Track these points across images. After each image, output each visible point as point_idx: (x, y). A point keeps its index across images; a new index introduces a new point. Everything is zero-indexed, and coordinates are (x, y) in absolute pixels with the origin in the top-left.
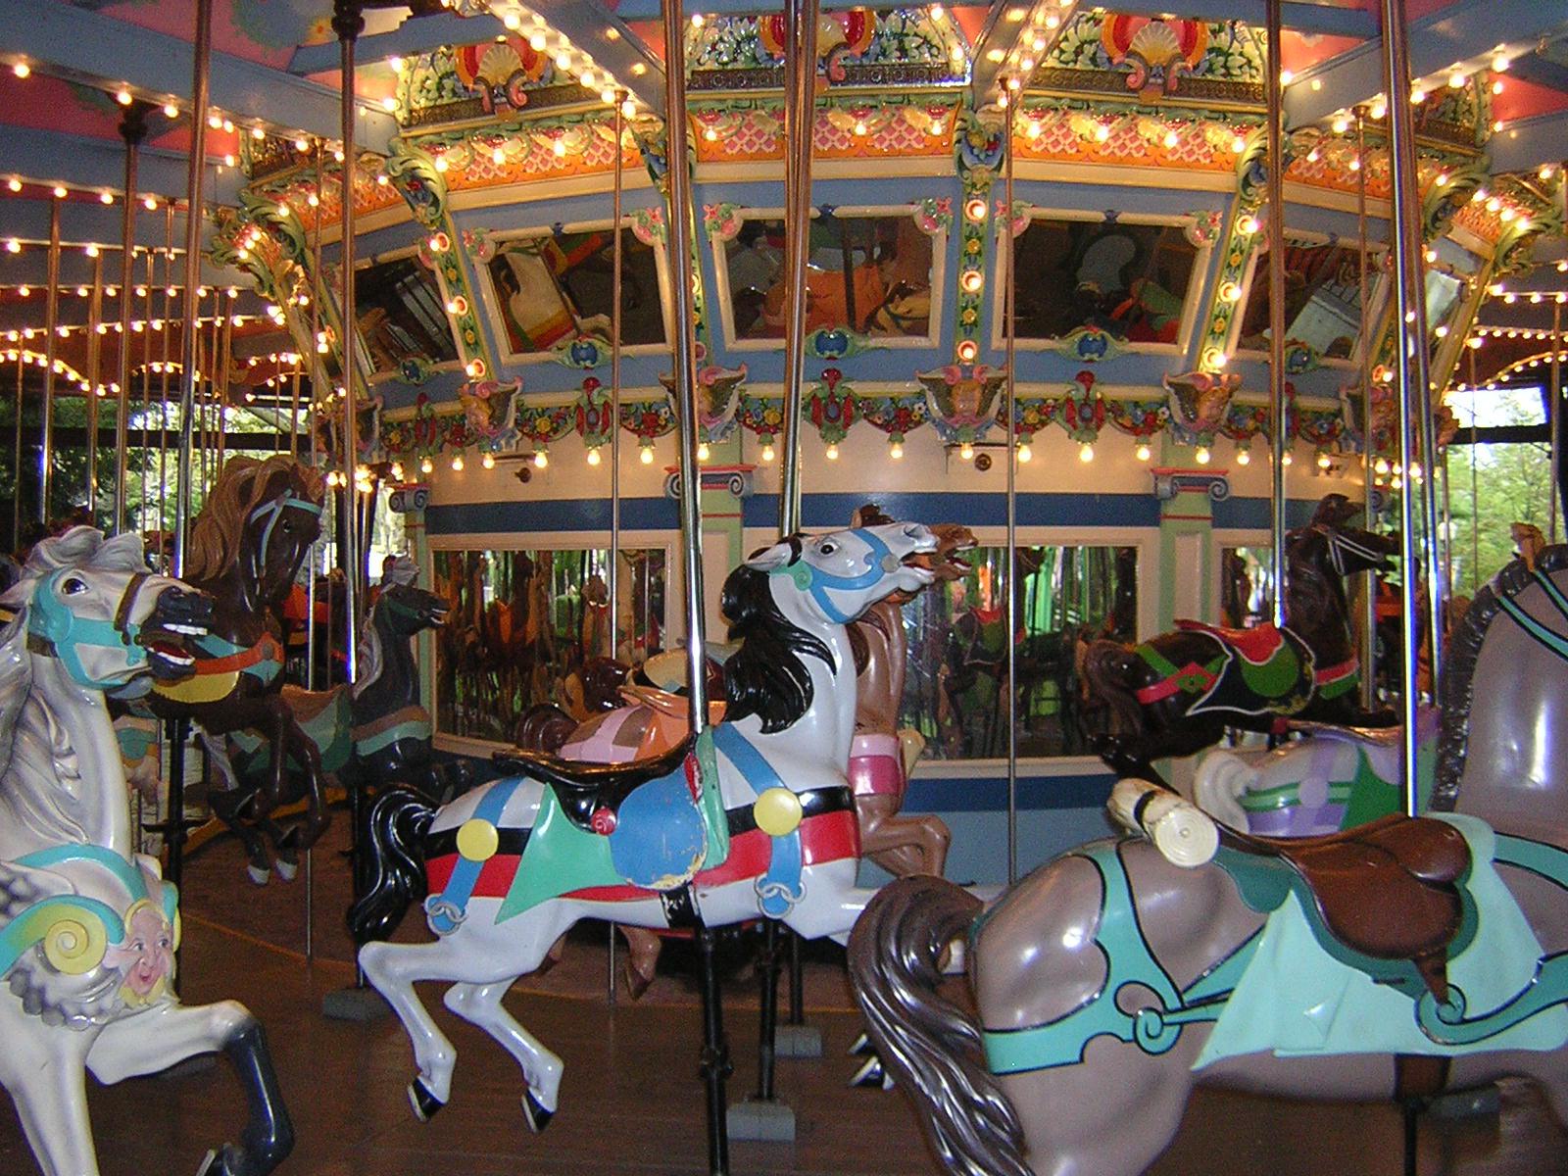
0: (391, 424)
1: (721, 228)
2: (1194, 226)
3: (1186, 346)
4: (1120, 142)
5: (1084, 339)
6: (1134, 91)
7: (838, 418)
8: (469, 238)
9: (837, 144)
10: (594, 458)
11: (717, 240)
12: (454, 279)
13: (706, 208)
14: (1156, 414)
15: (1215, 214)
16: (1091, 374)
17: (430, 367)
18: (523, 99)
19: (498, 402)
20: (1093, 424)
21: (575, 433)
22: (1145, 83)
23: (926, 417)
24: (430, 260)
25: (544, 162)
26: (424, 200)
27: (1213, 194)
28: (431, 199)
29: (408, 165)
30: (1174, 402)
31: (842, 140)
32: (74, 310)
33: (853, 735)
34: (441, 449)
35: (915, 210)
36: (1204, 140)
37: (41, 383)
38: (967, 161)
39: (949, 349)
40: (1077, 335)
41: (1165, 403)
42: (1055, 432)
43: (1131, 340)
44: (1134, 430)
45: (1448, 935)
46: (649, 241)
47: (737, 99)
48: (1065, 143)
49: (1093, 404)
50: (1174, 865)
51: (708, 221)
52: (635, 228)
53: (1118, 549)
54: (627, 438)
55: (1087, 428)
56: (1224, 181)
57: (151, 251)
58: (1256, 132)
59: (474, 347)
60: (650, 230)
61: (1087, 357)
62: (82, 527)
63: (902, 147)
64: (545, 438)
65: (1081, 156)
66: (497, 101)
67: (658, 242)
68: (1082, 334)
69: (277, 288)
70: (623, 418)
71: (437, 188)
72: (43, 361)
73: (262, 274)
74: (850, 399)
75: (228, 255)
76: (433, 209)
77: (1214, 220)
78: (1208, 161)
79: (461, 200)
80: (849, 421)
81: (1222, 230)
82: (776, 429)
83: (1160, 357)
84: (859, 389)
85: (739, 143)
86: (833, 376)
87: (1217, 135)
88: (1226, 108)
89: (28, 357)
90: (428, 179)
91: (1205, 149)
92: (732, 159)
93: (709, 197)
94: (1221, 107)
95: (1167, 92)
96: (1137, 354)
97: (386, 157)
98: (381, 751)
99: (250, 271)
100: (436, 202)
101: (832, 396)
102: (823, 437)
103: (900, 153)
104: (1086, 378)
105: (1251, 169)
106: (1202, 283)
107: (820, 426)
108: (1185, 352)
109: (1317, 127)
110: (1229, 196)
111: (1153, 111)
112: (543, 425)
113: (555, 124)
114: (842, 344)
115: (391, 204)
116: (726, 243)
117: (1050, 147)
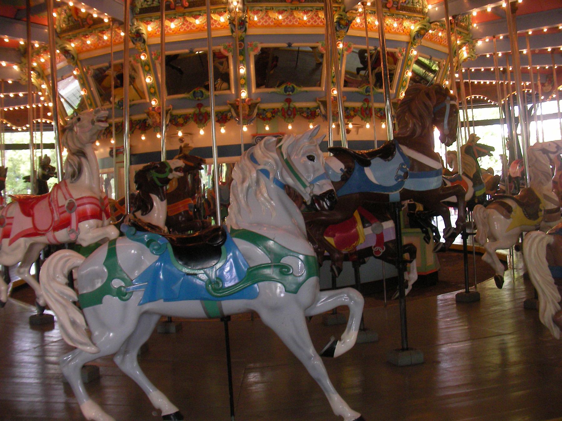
2: (398, 52)
3: (324, 88)
4: (289, 20)
5: (286, 88)
6: (389, 8)
7: (291, 115)
9: (295, 23)
10: (202, 132)
14: (315, 112)
15: (404, 48)
16: (290, 99)
18: (187, 4)
20: (292, 116)
22: (393, 6)
23: (232, 117)
25: (188, 27)
26: (140, 40)
27: (403, 42)
28: (143, 41)
29: (138, 28)
31: (296, 21)
35: (397, 50)
36: (294, 16)
38: (338, 29)
39: (328, 91)
40: (283, 87)
41: (230, 111)
43: (303, 87)
45: (320, 281)
46: (259, 49)
47: (267, 7)
48: (318, 21)
49: (292, 109)
50: (103, 298)
55: (290, 118)
56: (405, 38)
58: (419, 23)
61: (288, 93)
62: (406, 135)
63: (316, 24)
64: (182, 125)
65: (404, 33)
66: (177, 5)
68: (284, 86)
71: (145, 36)
74: (294, 108)
76: (143, 44)
77: (403, 50)
78: (322, 24)
81: (406, 53)
83: (318, 91)
84: (298, 105)
85: (262, 21)
86: (288, 101)
87: (406, 24)
88: (313, 5)
91: (320, 20)
92: (259, 27)
94: (311, 5)
95: (397, 9)
96: (307, 92)
100: (144, 42)
101: (289, 107)
103: (315, 26)
105: (416, 34)
108: (233, 92)
109: (438, 22)
110: (408, 43)
111: (392, 15)
112: (181, 121)
113: (198, 13)
114: (293, 90)
117: (186, 29)
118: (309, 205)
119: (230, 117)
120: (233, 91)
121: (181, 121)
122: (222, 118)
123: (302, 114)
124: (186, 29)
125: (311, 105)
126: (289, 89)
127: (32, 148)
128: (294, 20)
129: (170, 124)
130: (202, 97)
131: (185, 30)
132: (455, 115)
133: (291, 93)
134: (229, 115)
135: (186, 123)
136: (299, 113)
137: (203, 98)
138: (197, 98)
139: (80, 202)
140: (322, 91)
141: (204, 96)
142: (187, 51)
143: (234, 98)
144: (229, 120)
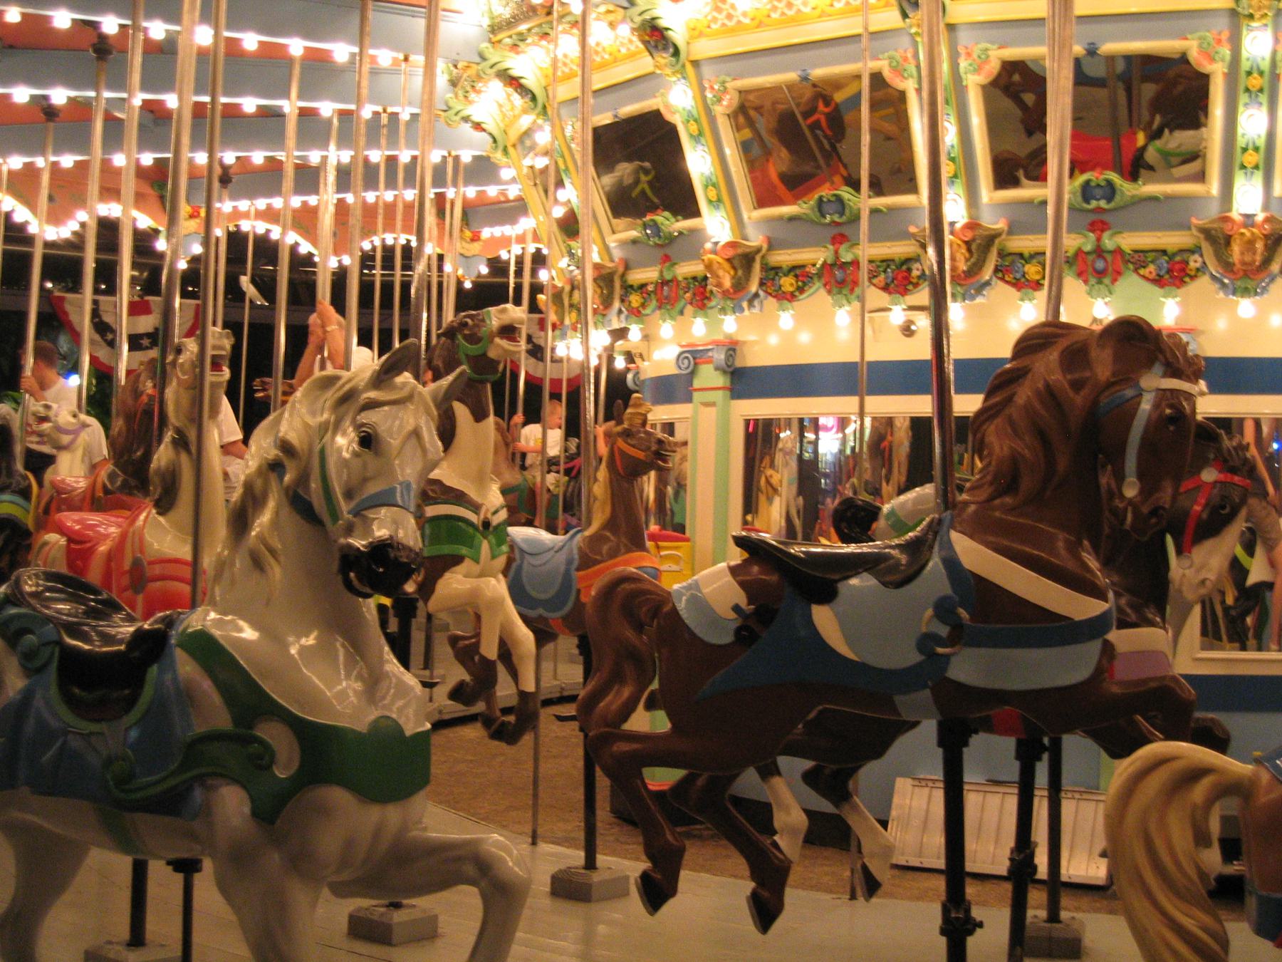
0: (631, 287)
1: (978, 70)
8: (712, 88)
11: (974, 82)
12: (696, 133)
13: (961, 50)
16: (1103, 222)
17: (674, 225)
19: (743, 260)
21: (823, 292)
23: (1202, 269)
24: (674, 113)
26: (665, 49)
28: (671, 50)
30: (1207, 249)
32: (308, 178)
33: (478, 635)
34: (681, 313)
37: (273, 259)
42: (818, 296)
44: (1158, 281)
46: (1207, 67)
51: (963, 64)
52: (887, 74)
53: (754, 420)
54: (875, 297)
57: (385, 111)
59: (716, 203)
60: (899, 71)
61: (1094, 204)
67: (909, 86)
68: (816, 196)
69: (511, 150)
70: (873, 276)
72: (276, 233)
73: (496, 133)
75: (462, 114)
79: (705, 49)
80: (1118, 274)
82: (1037, 285)
84: (1130, 241)
85: (719, 17)
89: (261, 227)
90: (667, 29)
93: (964, 37)
96: (1153, 199)
97: (625, 8)
98: (1014, 692)
99: (484, 130)
100: (676, 53)
102: (1089, 293)
104: (1099, 226)
106: (728, 151)
107: (1086, 282)
115: (632, 56)
116: (984, 87)
117: (726, 22)
118: (403, 589)
119: (919, 277)
120: (1214, 187)
121: (787, 283)
122: (1169, 271)
123: (1142, 271)
124: (726, 22)
125: (1172, 240)
126: (1098, 192)
127: (588, 368)
128: (719, 17)
129: (761, 293)
130: (842, 214)
131: (724, 25)
132: (972, 291)
133: (1103, 204)
134: (1194, 262)
135: (801, 290)
136: (1131, 266)
137: (1112, 205)
138: (828, 218)
139: (157, 570)
140: (1208, 197)
141: (847, 212)
142: (792, 76)
143: (1213, 211)
144: (1193, 278)
